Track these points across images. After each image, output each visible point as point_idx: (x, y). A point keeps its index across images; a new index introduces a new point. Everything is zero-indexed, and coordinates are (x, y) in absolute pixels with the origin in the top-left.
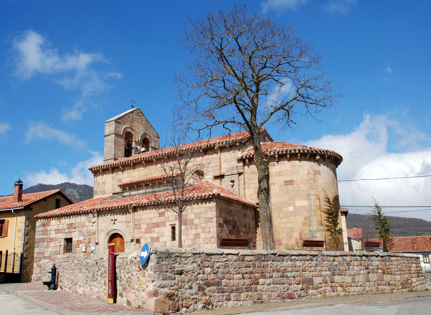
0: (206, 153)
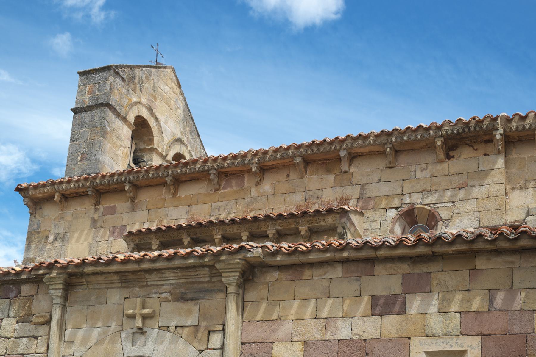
0: (451, 153)
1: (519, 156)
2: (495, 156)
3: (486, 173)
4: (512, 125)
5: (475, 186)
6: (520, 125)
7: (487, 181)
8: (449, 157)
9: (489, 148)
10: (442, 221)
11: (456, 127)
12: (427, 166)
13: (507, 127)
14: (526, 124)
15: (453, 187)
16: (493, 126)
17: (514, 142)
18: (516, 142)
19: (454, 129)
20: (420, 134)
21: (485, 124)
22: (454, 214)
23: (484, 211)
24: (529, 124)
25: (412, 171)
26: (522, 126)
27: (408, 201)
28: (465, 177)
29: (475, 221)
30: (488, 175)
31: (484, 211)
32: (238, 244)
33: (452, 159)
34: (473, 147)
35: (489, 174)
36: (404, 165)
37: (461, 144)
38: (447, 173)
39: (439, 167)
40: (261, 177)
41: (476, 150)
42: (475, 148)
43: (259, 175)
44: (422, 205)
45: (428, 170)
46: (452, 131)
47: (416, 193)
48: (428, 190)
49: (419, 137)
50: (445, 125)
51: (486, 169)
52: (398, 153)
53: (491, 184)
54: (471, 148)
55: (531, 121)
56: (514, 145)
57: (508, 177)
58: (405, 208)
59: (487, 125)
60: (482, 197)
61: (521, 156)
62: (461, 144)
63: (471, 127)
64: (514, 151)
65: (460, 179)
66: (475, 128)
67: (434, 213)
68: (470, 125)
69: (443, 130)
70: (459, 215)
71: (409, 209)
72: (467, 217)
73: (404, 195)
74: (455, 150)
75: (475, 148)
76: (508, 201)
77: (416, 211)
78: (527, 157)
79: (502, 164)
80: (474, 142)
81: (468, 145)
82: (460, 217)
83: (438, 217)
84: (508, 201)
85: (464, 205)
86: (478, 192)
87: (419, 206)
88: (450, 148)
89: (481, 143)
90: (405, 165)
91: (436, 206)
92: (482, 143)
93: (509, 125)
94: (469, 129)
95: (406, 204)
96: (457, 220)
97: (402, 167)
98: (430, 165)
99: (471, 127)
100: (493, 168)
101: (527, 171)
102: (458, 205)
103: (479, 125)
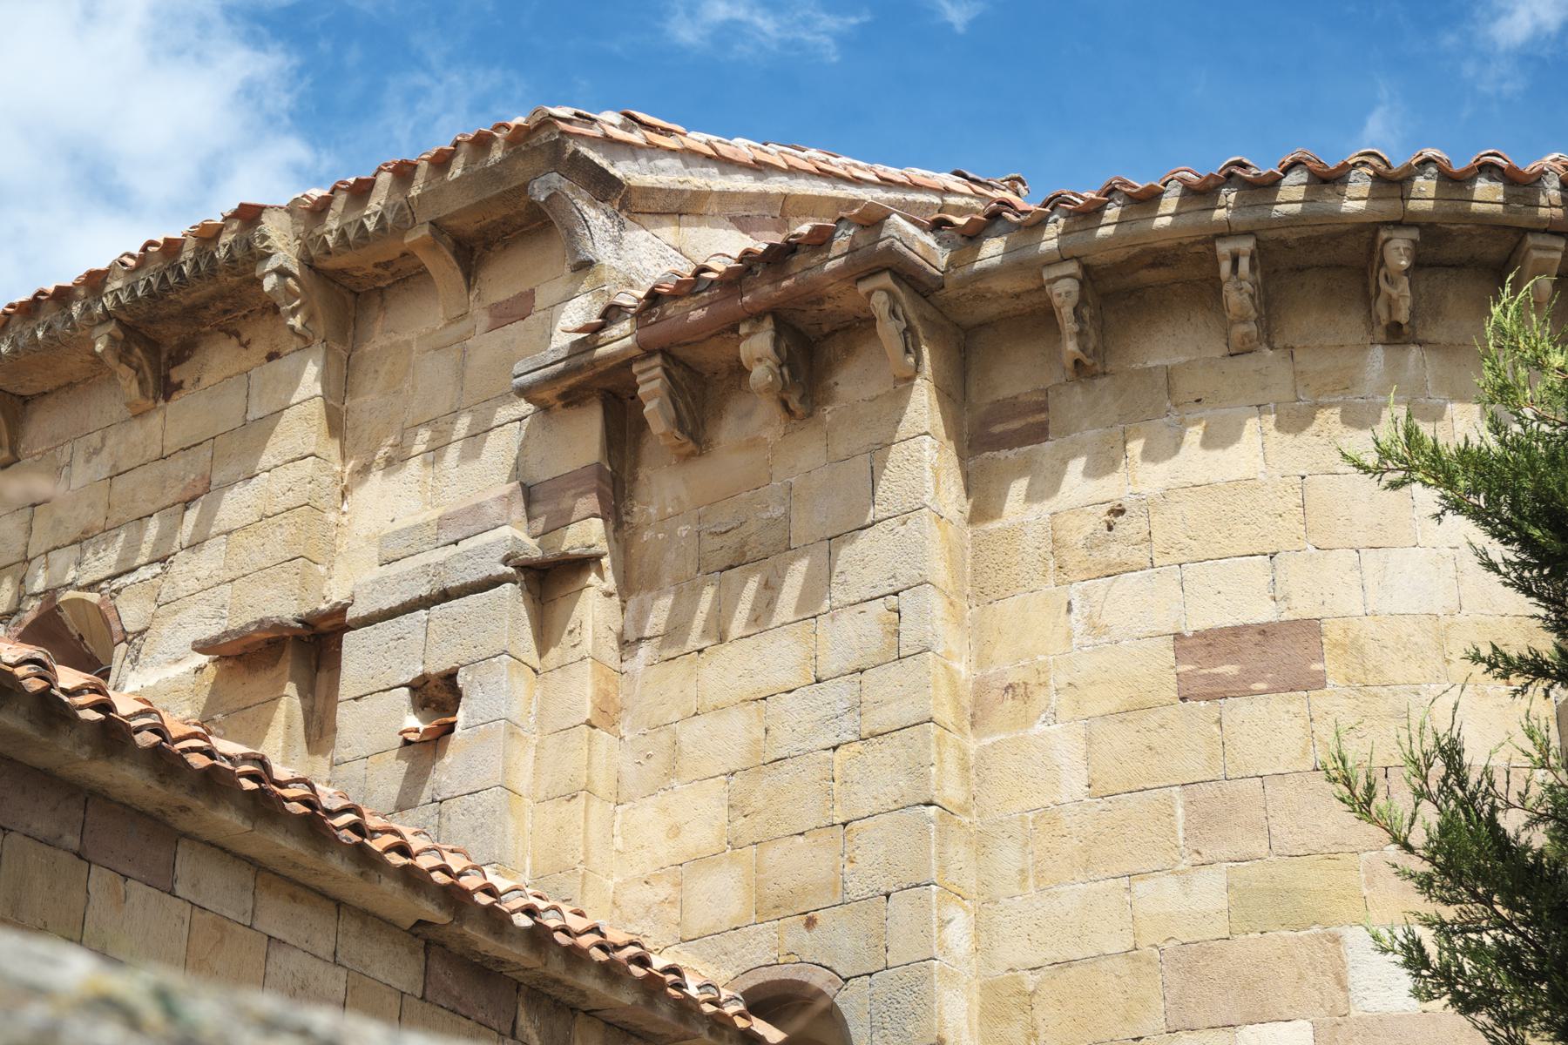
0: (176, 375)
1: (394, 339)
2: (298, 354)
3: (256, 430)
4: (327, 228)
5: (230, 485)
6: (350, 224)
7: (266, 459)
8: (167, 389)
9: (261, 336)
10: (125, 640)
11: (142, 275)
12: (103, 439)
13: (312, 240)
14: (368, 217)
15: (167, 502)
16: (249, 245)
17: (382, 290)
18: (389, 286)
19: (138, 282)
20: (44, 323)
21: (225, 246)
22: (159, 606)
23: (244, 576)
24: (376, 213)
25: (62, 464)
26: (358, 225)
27: (39, 585)
28: (204, 453)
29: (215, 621)
30: (270, 435)
31: (244, 576)
32: (362, 842)
33: (175, 396)
34: (238, 335)
35: (272, 429)
36: (40, 449)
37: (206, 334)
38: (157, 452)
39: (137, 432)
41: (245, 345)
42: (244, 339)
44: (79, 589)
45: (105, 453)
46: (133, 291)
47: (64, 546)
48: (98, 528)
49: (40, 334)
50: (111, 274)
51: (266, 412)
52: (29, 407)
53: (276, 466)
54: (234, 340)
55: (383, 202)
56: (383, 300)
57: (336, 424)
58: (32, 609)
59: (230, 246)
60: (244, 523)
61: (398, 337)
62: (206, 334)
63: (185, 263)
64: (378, 327)
65: (189, 467)
66: (196, 265)
67: (797, 608)
68: (182, 259)
69: (106, 295)
70: (173, 607)
71: (42, 612)
72: (193, 611)
73: (29, 562)
74: (188, 358)
75: (244, 339)
76: (344, 520)
77: (66, 615)
78: (415, 336)
79: (315, 380)
80: (245, 317)
81: (226, 331)
82: (176, 612)
83: (116, 627)
84: (344, 520)
85: (191, 566)
86: (236, 505)
87: (71, 594)
88: (174, 354)
89: (263, 314)
90: (45, 448)
91: (117, 584)
92: (266, 317)
93: (318, 231)
94: (180, 273)
95: (35, 595)
96: (165, 631)
97: (37, 457)
98: (112, 431)
99: (185, 263)
100: (286, 405)
101: (410, 393)
102: (175, 569)
103: (207, 253)
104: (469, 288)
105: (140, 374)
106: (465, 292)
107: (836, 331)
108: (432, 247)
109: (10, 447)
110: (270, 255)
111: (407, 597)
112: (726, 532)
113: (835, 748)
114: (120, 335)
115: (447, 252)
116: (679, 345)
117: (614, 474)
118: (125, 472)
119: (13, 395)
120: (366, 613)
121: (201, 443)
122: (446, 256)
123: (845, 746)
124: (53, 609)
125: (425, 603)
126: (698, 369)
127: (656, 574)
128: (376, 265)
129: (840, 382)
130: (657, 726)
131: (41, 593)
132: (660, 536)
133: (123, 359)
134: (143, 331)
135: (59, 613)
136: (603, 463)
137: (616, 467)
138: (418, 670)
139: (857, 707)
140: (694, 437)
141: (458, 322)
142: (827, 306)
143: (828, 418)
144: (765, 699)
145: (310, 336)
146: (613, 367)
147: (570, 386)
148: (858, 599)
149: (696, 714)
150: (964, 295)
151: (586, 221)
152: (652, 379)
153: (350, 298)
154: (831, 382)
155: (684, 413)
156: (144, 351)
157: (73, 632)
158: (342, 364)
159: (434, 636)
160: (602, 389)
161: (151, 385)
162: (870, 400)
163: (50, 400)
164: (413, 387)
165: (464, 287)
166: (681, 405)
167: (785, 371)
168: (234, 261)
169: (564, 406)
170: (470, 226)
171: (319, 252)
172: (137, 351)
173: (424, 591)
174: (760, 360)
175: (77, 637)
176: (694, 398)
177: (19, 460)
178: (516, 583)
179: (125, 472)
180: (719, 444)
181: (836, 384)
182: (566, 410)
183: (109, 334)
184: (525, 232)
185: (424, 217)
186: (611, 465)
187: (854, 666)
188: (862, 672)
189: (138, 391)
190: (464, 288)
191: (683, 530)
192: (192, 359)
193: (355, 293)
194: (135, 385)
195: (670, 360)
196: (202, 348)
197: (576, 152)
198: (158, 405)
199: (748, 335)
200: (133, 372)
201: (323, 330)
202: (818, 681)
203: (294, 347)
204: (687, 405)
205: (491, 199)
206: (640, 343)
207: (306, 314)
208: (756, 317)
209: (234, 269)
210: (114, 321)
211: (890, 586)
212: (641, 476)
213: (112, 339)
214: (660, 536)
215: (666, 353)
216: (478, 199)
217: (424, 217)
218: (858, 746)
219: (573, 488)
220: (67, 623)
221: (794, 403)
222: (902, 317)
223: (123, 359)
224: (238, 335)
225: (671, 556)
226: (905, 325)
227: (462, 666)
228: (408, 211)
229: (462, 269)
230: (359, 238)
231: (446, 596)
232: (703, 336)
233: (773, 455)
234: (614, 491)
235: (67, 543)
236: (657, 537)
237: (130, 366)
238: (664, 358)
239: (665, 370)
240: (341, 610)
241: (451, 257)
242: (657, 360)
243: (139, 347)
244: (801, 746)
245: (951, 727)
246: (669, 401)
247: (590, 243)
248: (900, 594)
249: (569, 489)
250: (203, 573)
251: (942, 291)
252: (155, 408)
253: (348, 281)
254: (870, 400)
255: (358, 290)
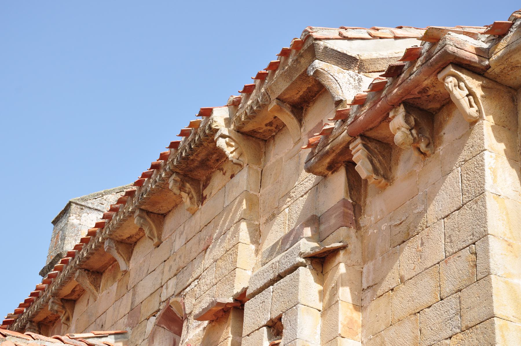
0: (206, 192)
40: (67, 315)
43: (62, 312)
104: (301, 126)
105: (190, 195)
106: (299, 129)
107: (444, 105)
108: (280, 110)
109: (158, 237)
110: (218, 130)
111: (266, 281)
112: (401, 223)
113: (450, 338)
114: (178, 178)
115: (287, 112)
116: (367, 131)
117: (354, 203)
118: (190, 240)
119: (159, 214)
120: (252, 291)
121: (211, 222)
122: (287, 113)
123: (455, 336)
124: (169, 307)
125: (272, 282)
126: (385, 141)
127: (374, 251)
128: (266, 125)
129: (445, 133)
130: (376, 334)
131: (166, 300)
132: (375, 231)
133: (182, 190)
134: (190, 176)
135: (171, 309)
136: (346, 198)
137: (355, 199)
138: (269, 317)
139: (460, 313)
140: (386, 177)
141: (298, 143)
142: (431, 93)
143: (441, 153)
144: (419, 312)
145: (242, 163)
146: (342, 148)
147: (329, 163)
148: (457, 250)
149: (391, 325)
150: (504, 68)
151: (337, 81)
152: (358, 151)
153: (261, 143)
154: (442, 133)
155: (378, 165)
156: (191, 185)
157: (179, 316)
158: (258, 174)
159: (274, 299)
160: (345, 161)
161: (196, 199)
162: (459, 139)
163: (171, 214)
164: (283, 178)
165: (298, 126)
166: (375, 161)
167: (414, 131)
168: (207, 136)
169: (332, 173)
170: (295, 96)
171: (239, 124)
172: (188, 185)
173: (271, 276)
174: (398, 129)
175: (181, 318)
176: (383, 156)
177: (162, 242)
178: (305, 266)
179: (190, 240)
180: (397, 178)
181: (444, 134)
182: (334, 174)
183: (174, 180)
184: (320, 94)
185: (273, 97)
186: (351, 199)
187: (457, 288)
188: (460, 291)
189: (189, 202)
190: (298, 126)
191: (383, 227)
192: (209, 185)
193: (265, 140)
194: (188, 200)
195: (366, 140)
196: (212, 179)
197: (326, 48)
198: (199, 208)
199: (394, 117)
200: (187, 195)
201: (247, 160)
202: (442, 299)
203: (238, 170)
204: (379, 161)
205: (296, 80)
206: (350, 134)
207: (238, 153)
208: (394, 106)
209: (208, 139)
210: (175, 173)
211: (471, 239)
212: (368, 202)
213: (175, 181)
214: (375, 231)
215: (363, 136)
216: (291, 82)
217: (273, 97)
218: (461, 335)
219: (334, 213)
220: (176, 312)
221: (422, 146)
222: (465, 88)
223: (182, 190)
224: (222, 170)
225: (379, 241)
226: (467, 92)
227: (283, 312)
228: (267, 96)
229: (297, 118)
230: (251, 113)
231: (280, 277)
232: (376, 123)
233: (419, 179)
234: (354, 212)
235: (172, 276)
236: (374, 232)
237: (185, 192)
238: (362, 139)
239: (365, 145)
240: (245, 290)
241: (290, 113)
242: (359, 140)
243: (189, 183)
244: (435, 338)
245: (512, 319)
246: (368, 161)
247: (340, 91)
248: (476, 243)
249: (333, 214)
250: (208, 282)
251: (490, 70)
252: (198, 209)
253: (258, 135)
254: (459, 139)
255: (265, 139)
